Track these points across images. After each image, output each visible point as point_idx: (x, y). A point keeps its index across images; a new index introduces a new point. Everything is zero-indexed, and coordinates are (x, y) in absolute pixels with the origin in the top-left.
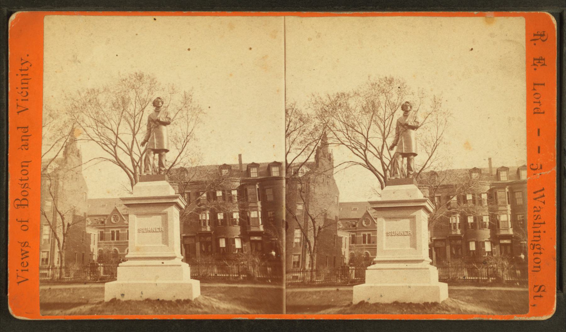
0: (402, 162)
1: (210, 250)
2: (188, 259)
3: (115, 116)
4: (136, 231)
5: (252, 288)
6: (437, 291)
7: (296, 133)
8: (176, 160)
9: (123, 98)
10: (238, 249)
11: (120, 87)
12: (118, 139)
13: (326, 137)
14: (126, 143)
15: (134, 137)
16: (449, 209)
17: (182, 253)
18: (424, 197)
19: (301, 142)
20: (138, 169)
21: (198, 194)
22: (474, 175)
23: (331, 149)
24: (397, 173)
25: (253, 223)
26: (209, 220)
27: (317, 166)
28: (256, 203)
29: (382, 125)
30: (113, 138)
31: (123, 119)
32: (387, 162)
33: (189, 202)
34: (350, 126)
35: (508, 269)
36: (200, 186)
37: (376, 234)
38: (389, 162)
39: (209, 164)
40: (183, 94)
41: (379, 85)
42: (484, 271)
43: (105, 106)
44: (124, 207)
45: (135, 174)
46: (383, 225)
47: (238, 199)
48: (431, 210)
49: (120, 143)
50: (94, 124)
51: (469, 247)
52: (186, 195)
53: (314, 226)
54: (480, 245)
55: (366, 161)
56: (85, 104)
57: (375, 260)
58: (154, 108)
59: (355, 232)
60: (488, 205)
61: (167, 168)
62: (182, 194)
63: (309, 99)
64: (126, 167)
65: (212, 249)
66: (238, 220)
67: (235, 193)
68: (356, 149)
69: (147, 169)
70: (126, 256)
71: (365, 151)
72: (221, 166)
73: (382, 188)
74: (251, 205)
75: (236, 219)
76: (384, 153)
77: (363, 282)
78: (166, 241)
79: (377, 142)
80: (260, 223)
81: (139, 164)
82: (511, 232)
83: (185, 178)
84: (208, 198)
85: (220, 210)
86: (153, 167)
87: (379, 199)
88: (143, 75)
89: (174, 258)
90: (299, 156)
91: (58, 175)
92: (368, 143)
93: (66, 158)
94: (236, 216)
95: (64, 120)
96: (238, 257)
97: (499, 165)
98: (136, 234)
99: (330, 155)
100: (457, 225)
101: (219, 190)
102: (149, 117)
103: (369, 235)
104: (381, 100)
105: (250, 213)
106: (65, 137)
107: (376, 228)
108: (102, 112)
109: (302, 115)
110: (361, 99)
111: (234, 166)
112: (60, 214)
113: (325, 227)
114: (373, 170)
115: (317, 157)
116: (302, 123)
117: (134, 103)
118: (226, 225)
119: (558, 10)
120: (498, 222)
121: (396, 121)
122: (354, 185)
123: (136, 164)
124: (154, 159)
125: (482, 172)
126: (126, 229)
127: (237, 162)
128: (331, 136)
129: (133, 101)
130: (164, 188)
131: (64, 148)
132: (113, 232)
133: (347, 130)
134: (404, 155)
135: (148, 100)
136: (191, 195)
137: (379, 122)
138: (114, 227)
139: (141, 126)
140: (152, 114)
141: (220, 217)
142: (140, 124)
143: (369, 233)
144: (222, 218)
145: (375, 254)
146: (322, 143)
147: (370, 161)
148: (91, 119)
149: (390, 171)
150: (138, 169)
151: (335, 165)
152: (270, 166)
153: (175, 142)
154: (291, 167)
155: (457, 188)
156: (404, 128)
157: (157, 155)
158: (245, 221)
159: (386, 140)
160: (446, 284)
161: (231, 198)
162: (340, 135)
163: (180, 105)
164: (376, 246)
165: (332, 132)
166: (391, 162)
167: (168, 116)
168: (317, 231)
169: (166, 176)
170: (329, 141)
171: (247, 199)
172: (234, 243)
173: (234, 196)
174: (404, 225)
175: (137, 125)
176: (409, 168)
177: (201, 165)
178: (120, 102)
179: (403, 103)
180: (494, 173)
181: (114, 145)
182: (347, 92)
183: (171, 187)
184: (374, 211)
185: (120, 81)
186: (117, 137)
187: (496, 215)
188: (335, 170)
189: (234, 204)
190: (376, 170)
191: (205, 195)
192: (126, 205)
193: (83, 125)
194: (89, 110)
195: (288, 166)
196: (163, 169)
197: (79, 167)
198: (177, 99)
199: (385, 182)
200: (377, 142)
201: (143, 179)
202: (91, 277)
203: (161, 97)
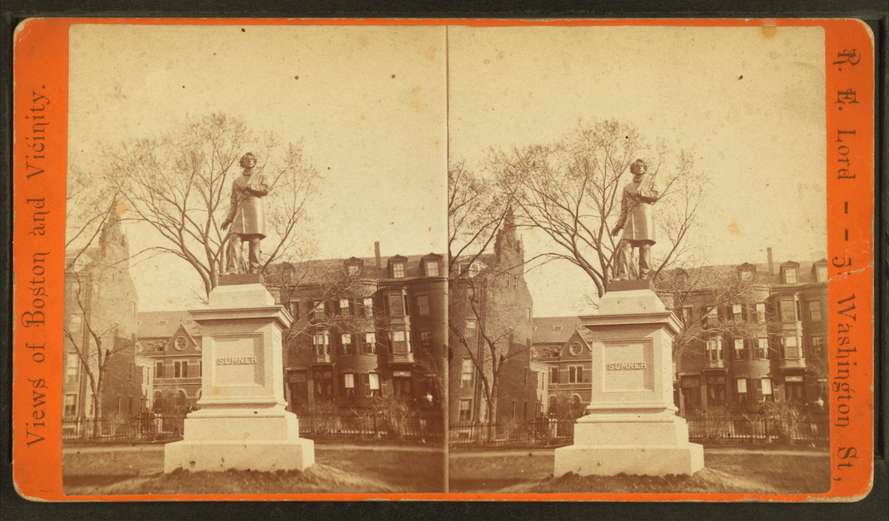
0: (632, 255)
1: (329, 392)
2: (296, 404)
3: (180, 181)
5: (396, 452)
6: (686, 457)
7: (465, 208)
8: (277, 251)
10: (375, 391)
11: (189, 136)
12: (185, 219)
13: (512, 215)
14: (198, 225)
15: (210, 215)
16: (706, 328)
17: (285, 397)
18: (667, 309)
19: (473, 223)
20: (216, 265)
21: (310, 305)
22: (745, 275)
23: (125, 227)
25: (397, 351)
27: (499, 261)
28: (402, 318)
29: (600, 197)
30: (178, 217)
32: (608, 254)
33: (297, 317)
35: (797, 422)
36: (314, 292)
37: (590, 367)
38: (218, 248)
40: (288, 147)
41: (595, 134)
42: (761, 425)
43: (165, 167)
44: (194, 324)
45: (211, 274)
46: (602, 354)
47: (374, 313)
48: (677, 329)
49: (188, 225)
50: (147, 195)
51: (737, 388)
52: (292, 306)
53: (494, 355)
54: (754, 385)
55: (575, 252)
56: (133, 164)
57: (588, 407)
58: (242, 170)
59: (164, 358)
61: (263, 264)
62: (287, 305)
63: (486, 156)
64: (197, 262)
65: (332, 391)
66: (373, 346)
67: (368, 302)
69: (230, 265)
70: (198, 402)
73: (600, 295)
74: (394, 321)
75: (370, 344)
76: (603, 240)
77: (570, 442)
78: (260, 378)
79: (199, 215)
80: (409, 349)
81: (219, 257)
82: (802, 364)
83: (290, 279)
84: (327, 311)
85: (346, 330)
86: (241, 263)
87: (596, 313)
88: (224, 118)
89: (273, 404)
90: (469, 246)
91: (90, 275)
93: (104, 248)
94: (371, 338)
96: (374, 403)
97: (784, 260)
99: (518, 242)
100: (718, 353)
101: (344, 298)
102: (235, 184)
103: (580, 369)
104: (598, 158)
105: (392, 335)
106: (102, 214)
107: (591, 357)
108: (161, 176)
109: (474, 181)
110: (567, 155)
111: (368, 260)
112: (94, 335)
114: (587, 267)
115: (497, 247)
116: (475, 194)
117: (210, 162)
118: (355, 352)
119: (876, 16)
120: (782, 349)
121: (622, 190)
122: (555, 290)
123: (213, 257)
124: (242, 249)
125: (758, 270)
126: (199, 360)
127: (372, 255)
128: (520, 213)
129: (209, 158)
130: (258, 296)
131: (100, 232)
132: (177, 364)
133: (545, 204)
134: (635, 244)
135: (232, 157)
136: (301, 305)
137: (596, 192)
138: (178, 356)
139: (221, 197)
140: (239, 179)
141: (346, 340)
143: (580, 365)
144: (349, 341)
145: (589, 399)
146: (505, 225)
147: (582, 253)
148: (143, 187)
149: (613, 269)
150: (216, 265)
151: (526, 259)
152: (424, 261)
153: (275, 222)
154: (458, 263)
156: (634, 201)
157: (246, 244)
158: (385, 347)
159: (607, 220)
160: (701, 446)
161: (363, 311)
162: (534, 211)
163: (283, 165)
164: (591, 386)
165: (521, 208)
166: (614, 254)
167: (264, 182)
168: (497, 363)
169: (261, 276)
170: (517, 222)
171: (388, 313)
172: (368, 381)
173: (368, 307)
174: (634, 352)
175: (216, 196)
176: (643, 264)
177: (709, 265)
179: (634, 161)
180: (777, 271)
181: (179, 227)
182: (546, 145)
183: (268, 294)
184: (588, 330)
187: (779, 338)
188: (526, 267)
189: (367, 320)
190: (590, 267)
191: (322, 306)
192: (198, 321)
194: (140, 173)
195: (452, 261)
196: (256, 265)
197: (125, 262)
198: (279, 155)
199: (605, 286)
200: (592, 222)
201: (225, 281)
202: (142, 434)
203: (253, 153)
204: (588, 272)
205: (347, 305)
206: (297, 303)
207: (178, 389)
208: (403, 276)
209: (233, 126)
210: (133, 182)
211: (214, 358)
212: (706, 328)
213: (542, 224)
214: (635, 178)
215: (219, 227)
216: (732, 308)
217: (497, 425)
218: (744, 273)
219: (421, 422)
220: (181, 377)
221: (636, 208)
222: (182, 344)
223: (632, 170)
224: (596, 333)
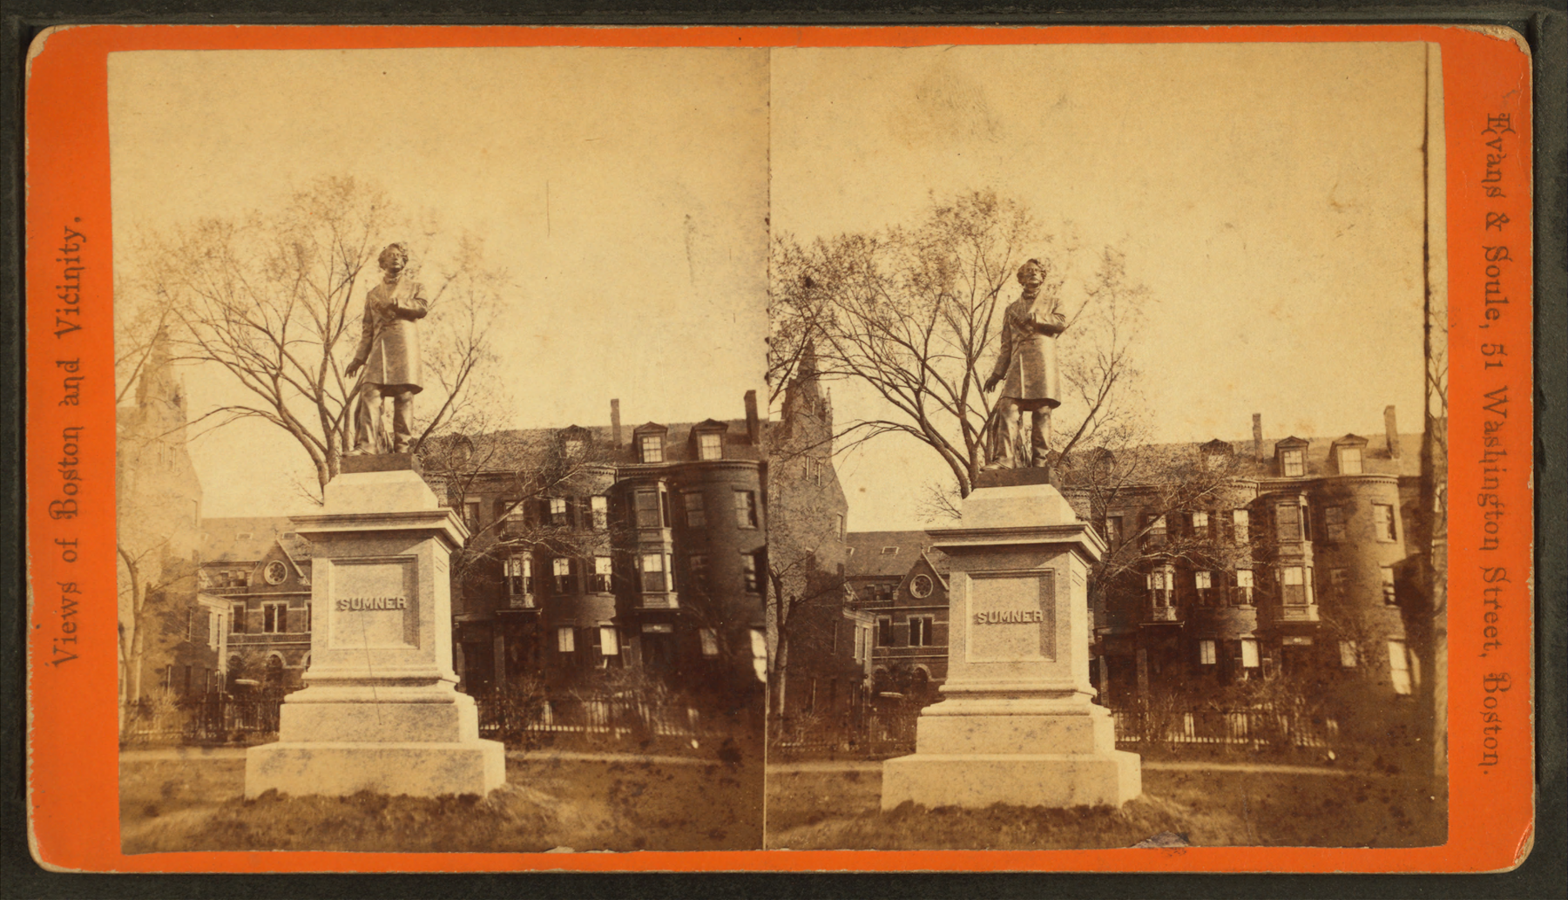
0: (1019, 424)
2: (471, 684)
4: (970, 621)
6: (467, 760)
8: (1083, 427)
9: (940, 260)
10: (610, 657)
12: (927, 372)
15: (327, 352)
17: (455, 668)
20: (337, 438)
21: (500, 507)
24: (366, 440)
26: (1173, 592)
28: (658, 531)
30: (914, 369)
31: (298, 303)
32: (977, 424)
33: (475, 530)
34: (879, 326)
35: (665, 703)
36: (505, 487)
37: (946, 619)
39: (531, 426)
43: (891, 283)
45: (328, 452)
46: (969, 596)
47: (609, 522)
49: (932, 383)
51: (557, 643)
52: (467, 510)
53: (779, 597)
54: (1228, 653)
55: (921, 420)
57: (942, 688)
58: (383, 273)
60: (1252, 543)
61: (418, 436)
62: (458, 508)
66: (607, 579)
67: (599, 504)
68: (895, 387)
69: (361, 440)
70: (305, 675)
71: (917, 393)
72: (561, 431)
73: (964, 494)
76: (969, 400)
78: (413, 631)
80: (670, 586)
81: (341, 425)
82: (1313, 614)
83: (464, 461)
84: (1171, 531)
86: (379, 434)
87: (955, 525)
89: (434, 680)
92: (927, 372)
94: (603, 566)
95: (779, 318)
98: (333, 615)
100: (1168, 595)
101: (558, 497)
103: (927, 622)
105: (641, 561)
106: (785, 363)
107: (947, 601)
111: (598, 430)
112: (126, 557)
113: (808, 597)
115: (786, 408)
117: (970, 275)
118: (1217, 602)
119: (1521, 14)
120: (1279, 588)
123: (332, 425)
124: (381, 410)
127: (1248, 435)
128: (827, 352)
129: (967, 268)
131: (138, 379)
136: (482, 508)
137: (956, 314)
138: (273, 598)
142: (985, 332)
144: (566, 571)
147: (931, 419)
149: (986, 450)
150: (337, 438)
151: (835, 432)
153: (438, 366)
155: (523, 480)
156: (385, 319)
157: (389, 401)
158: (628, 581)
159: (333, 351)
160: (501, 745)
162: (851, 349)
163: (1095, 283)
164: (946, 651)
166: (987, 426)
169: (414, 458)
170: (822, 366)
171: (633, 523)
172: (598, 640)
173: (598, 512)
175: (979, 333)
176: (1038, 441)
177: (510, 428)
178: (292, 258)
179: (1024, 262)
181: (916, 387)
183: (426, 488)
185: (934, 214)
186: (924, 365)
187: (630, 559)
188: (837, 445)
191: (518, 510)
193: (189, 317)
194: (850, 293)
196: (406, 439)
197: (180, 432)
199: (971, 479)
200: (951, 367)
201: (350, 465)
202: (208, 731)
204: (943, 454)
205: (1205, 523)
206: (477, 504)
207: (271, 653)
208: (659, 459)
209: (1011, 215)
210: (837, 309)
211: (969, 612)
212: (1145, 553)
213: (221, 355)
214: (1026, 291)
215: (341, 372)
216: (548, 504)
217: (786, 718)
218: (569, 443)
219: (691, 712)
220: (276, 632)
221: (1027, 346)
222: (923, 587)
223: (1021, 277)
224: (956, 559)
